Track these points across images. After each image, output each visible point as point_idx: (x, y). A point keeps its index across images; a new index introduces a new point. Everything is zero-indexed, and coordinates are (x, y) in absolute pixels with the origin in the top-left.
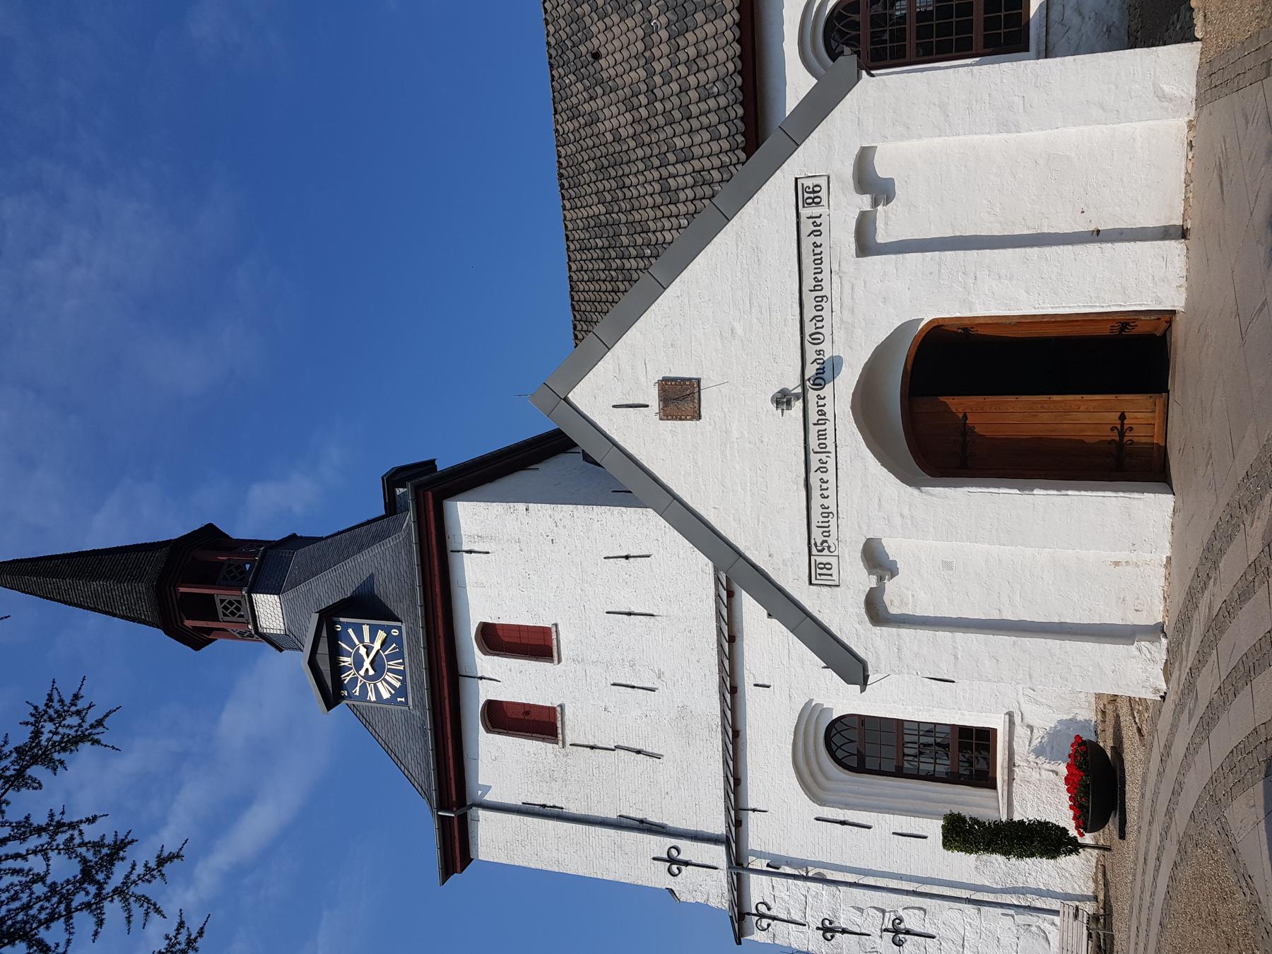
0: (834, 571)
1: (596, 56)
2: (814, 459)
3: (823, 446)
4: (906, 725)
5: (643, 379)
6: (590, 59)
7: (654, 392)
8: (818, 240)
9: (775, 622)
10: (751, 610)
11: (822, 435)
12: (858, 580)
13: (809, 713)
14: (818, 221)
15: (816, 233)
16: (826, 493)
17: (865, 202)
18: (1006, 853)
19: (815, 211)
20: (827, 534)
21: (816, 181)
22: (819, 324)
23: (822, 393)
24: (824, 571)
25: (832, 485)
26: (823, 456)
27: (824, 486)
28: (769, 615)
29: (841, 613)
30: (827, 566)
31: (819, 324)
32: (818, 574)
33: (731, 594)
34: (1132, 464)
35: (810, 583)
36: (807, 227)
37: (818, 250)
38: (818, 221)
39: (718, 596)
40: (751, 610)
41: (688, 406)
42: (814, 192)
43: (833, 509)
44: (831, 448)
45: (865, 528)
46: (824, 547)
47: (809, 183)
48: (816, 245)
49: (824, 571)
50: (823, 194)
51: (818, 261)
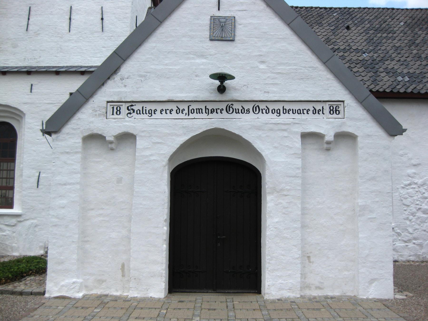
0: (115, 116)
1: (348, 28)
2: (184, 106)
3: (193, 111)
4: (12, 164)
5: (237, 8)
6: (346, 25)
7: (228, 14)
8: (311, 112)
9: (67, 97)
10: (75, 84)
11: (199, 111)
12: (113, 126)
13: (18, 114)
14: (321, 113)
15: (315, 111)
16: (164, 112)
17: (330, 137)
18: (31, 256)
19: (327, 110)
20: (139, 112)
21: (342, 112)
22: (264, 111)
23: (224, 112)
24: (115, 110)
25: (169, 116)
26: (186, 111)
27: (168, 112)
28: (71, 94)
29: (88, 119)
30: (119, 112)
31: (264, 111)
32: (116, 107)
33: (83, 73)
34: (183, 276)
35: (108, 102)
36: (318, 107)
37: (305, 112)
38: (321, 113)
39: (81, 67)
40: (75, 84)
41: (218, 33)
42: (336, 110)
43: (154, 116)
44: (191, 116)
45: (143, 134)
46: (131, 111)
47: (341, 109)
48: (308, 111)
49: (115, 110)
50: (335, 115)
51: (300, 112)
